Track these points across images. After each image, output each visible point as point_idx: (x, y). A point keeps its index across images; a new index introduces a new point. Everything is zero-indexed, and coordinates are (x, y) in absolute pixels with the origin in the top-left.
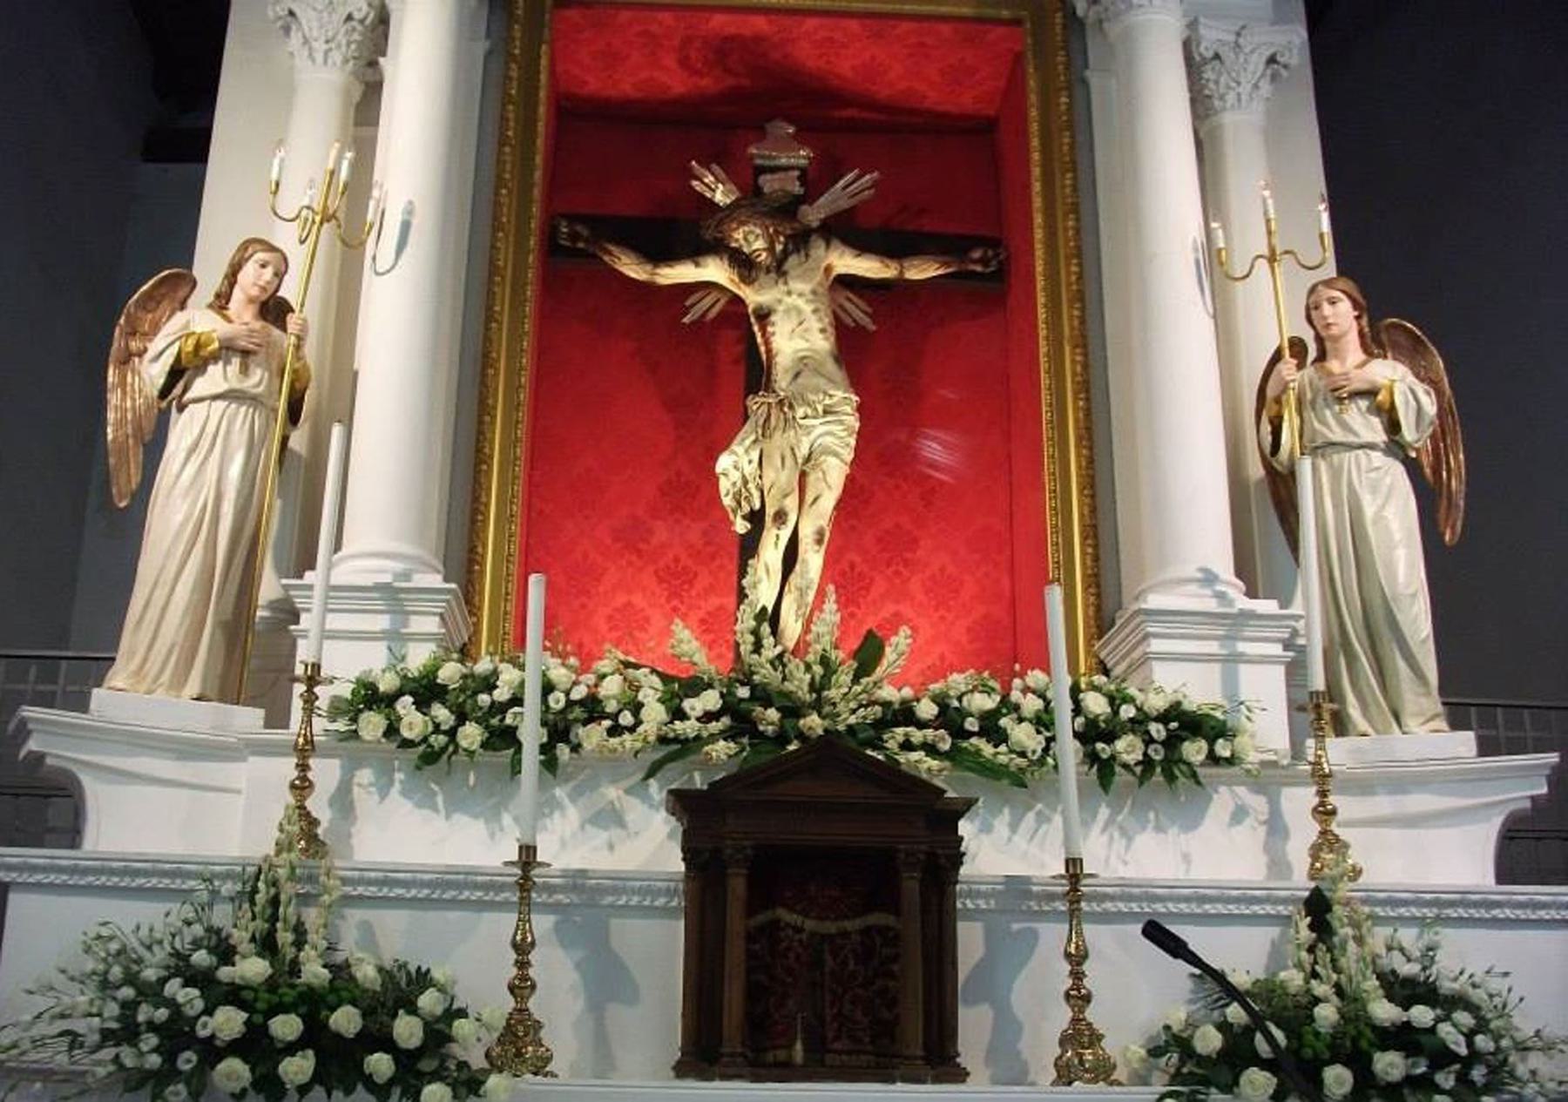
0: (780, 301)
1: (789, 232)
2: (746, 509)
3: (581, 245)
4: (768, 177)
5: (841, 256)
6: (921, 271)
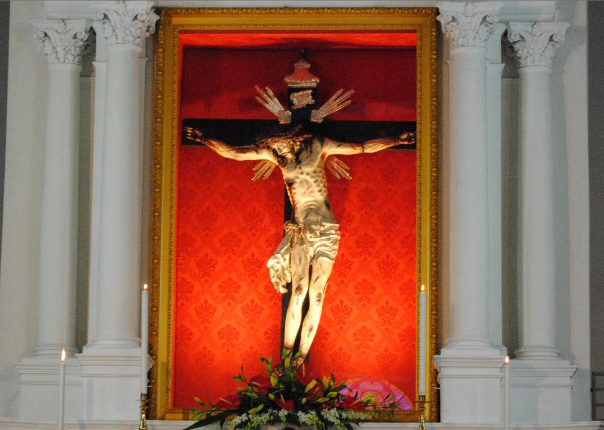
0: (297, 177)
1: (301, 139)
2: (284, 283)
3: (198, 140)
4: (296, 94)
5: (329, 148)
6: (374, 148)
